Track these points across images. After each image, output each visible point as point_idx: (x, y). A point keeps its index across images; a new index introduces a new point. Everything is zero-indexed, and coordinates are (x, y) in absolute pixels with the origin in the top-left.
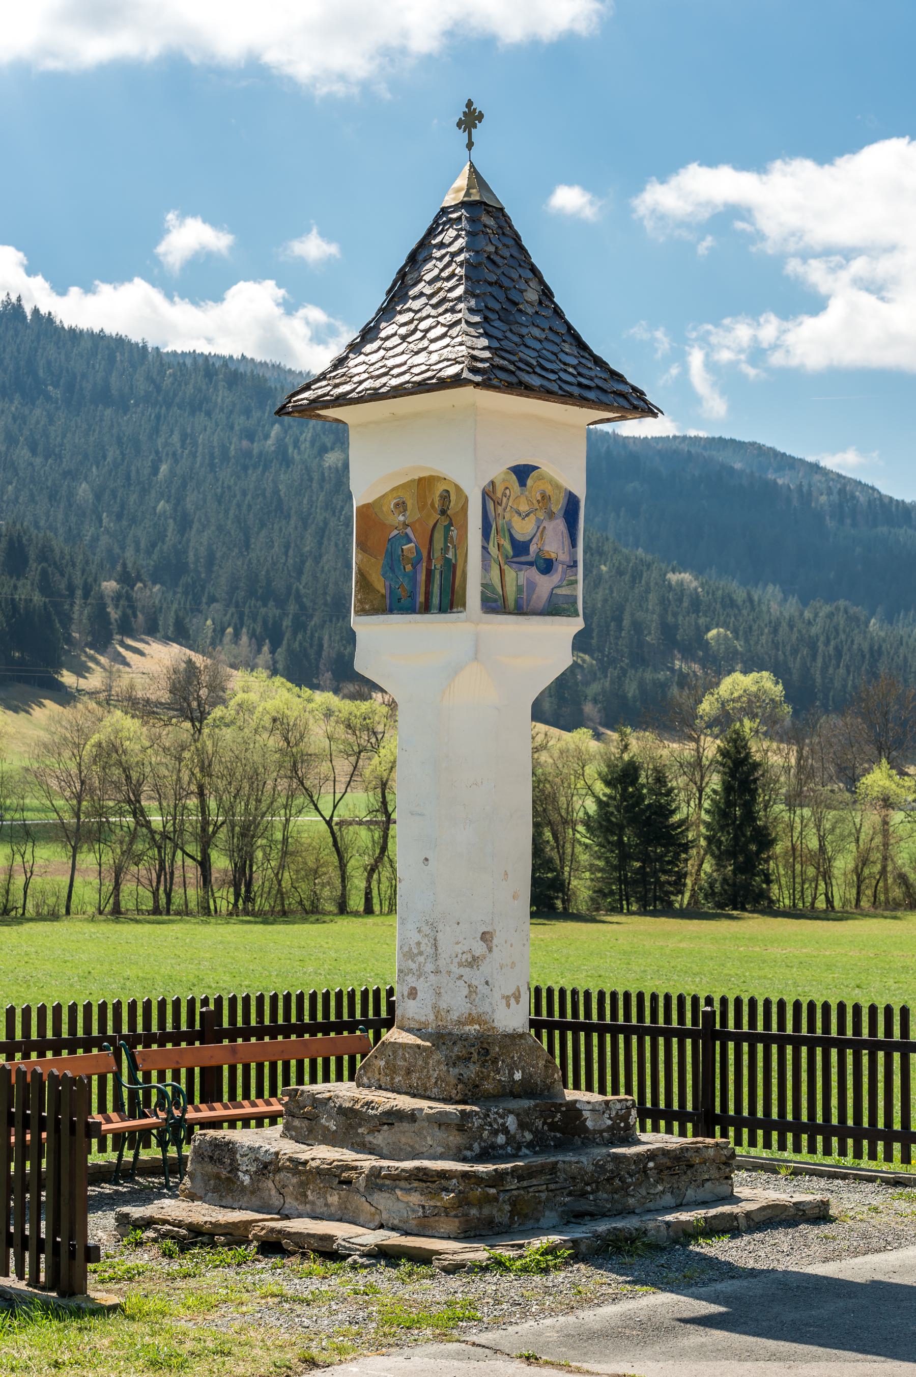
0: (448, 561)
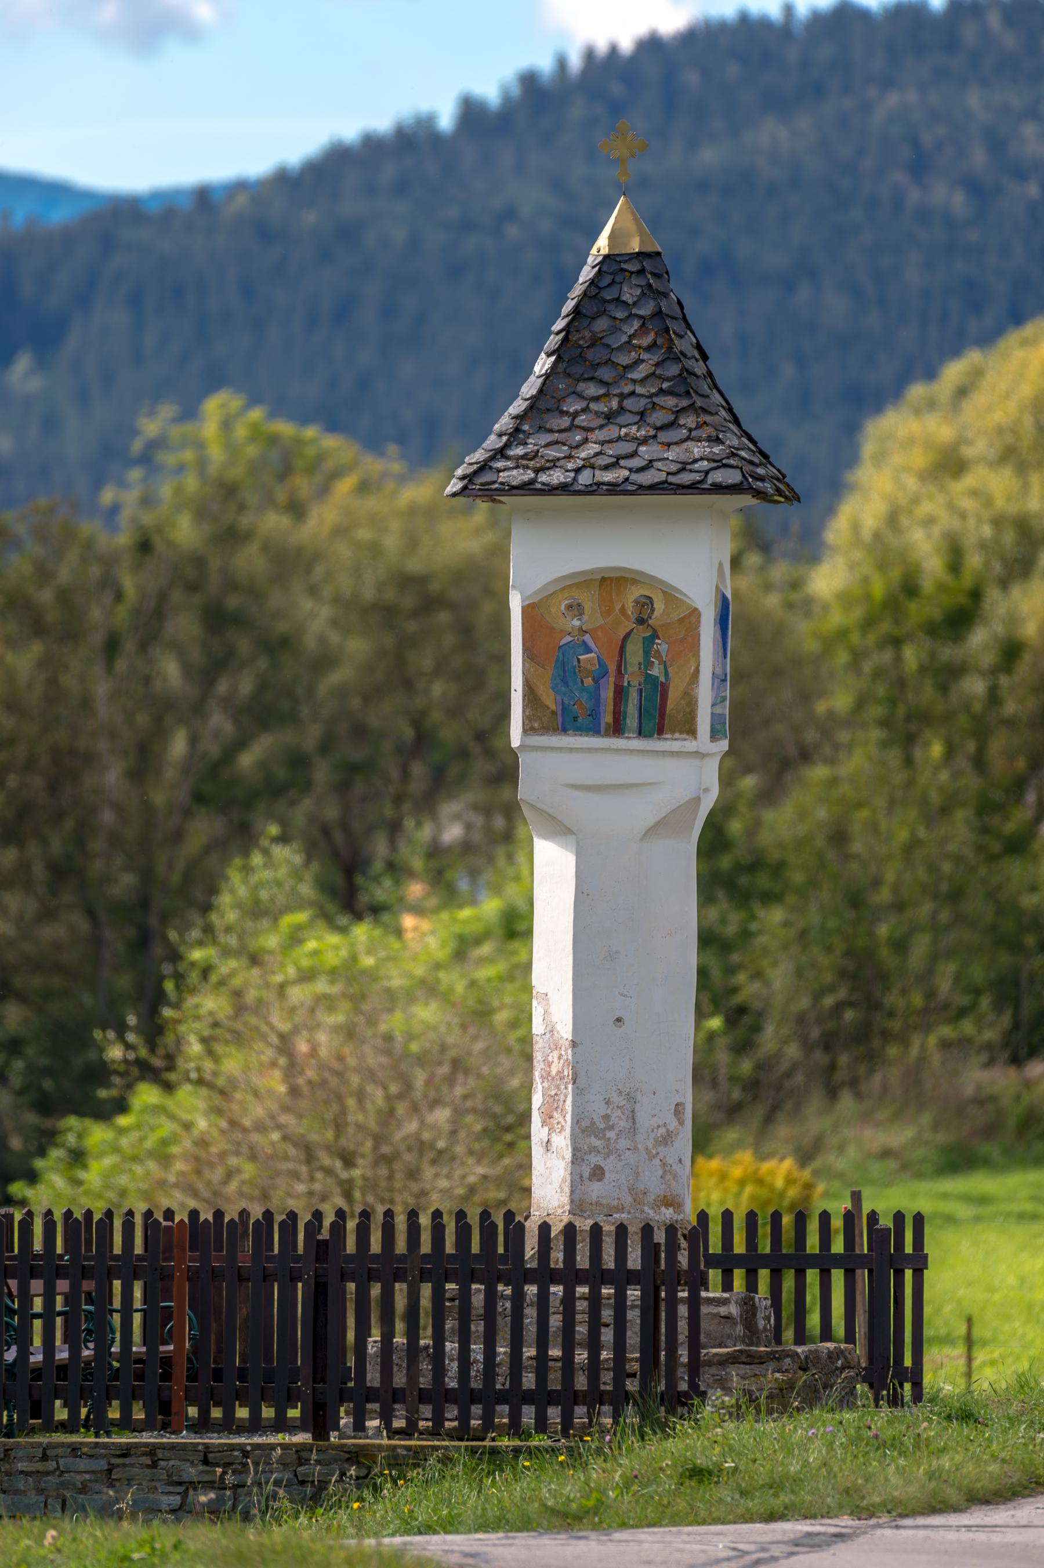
0: (651, 680)
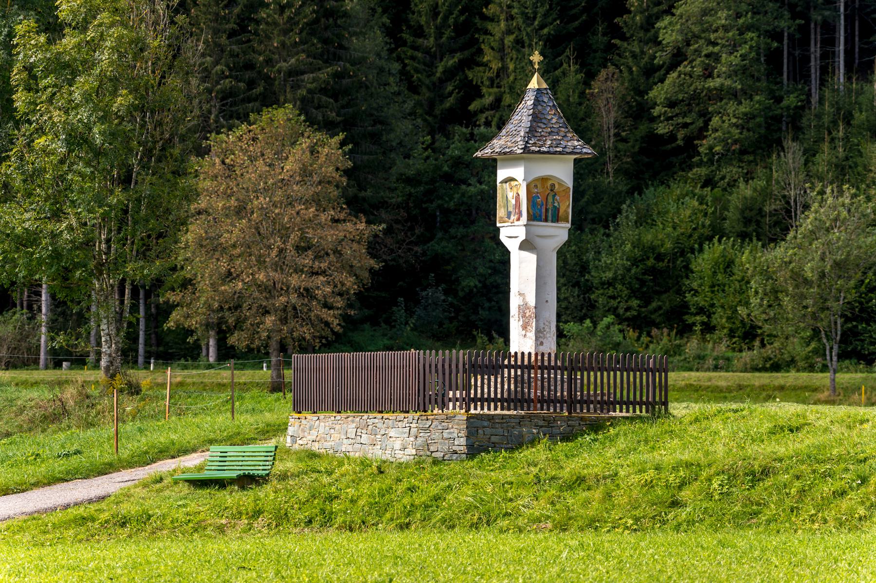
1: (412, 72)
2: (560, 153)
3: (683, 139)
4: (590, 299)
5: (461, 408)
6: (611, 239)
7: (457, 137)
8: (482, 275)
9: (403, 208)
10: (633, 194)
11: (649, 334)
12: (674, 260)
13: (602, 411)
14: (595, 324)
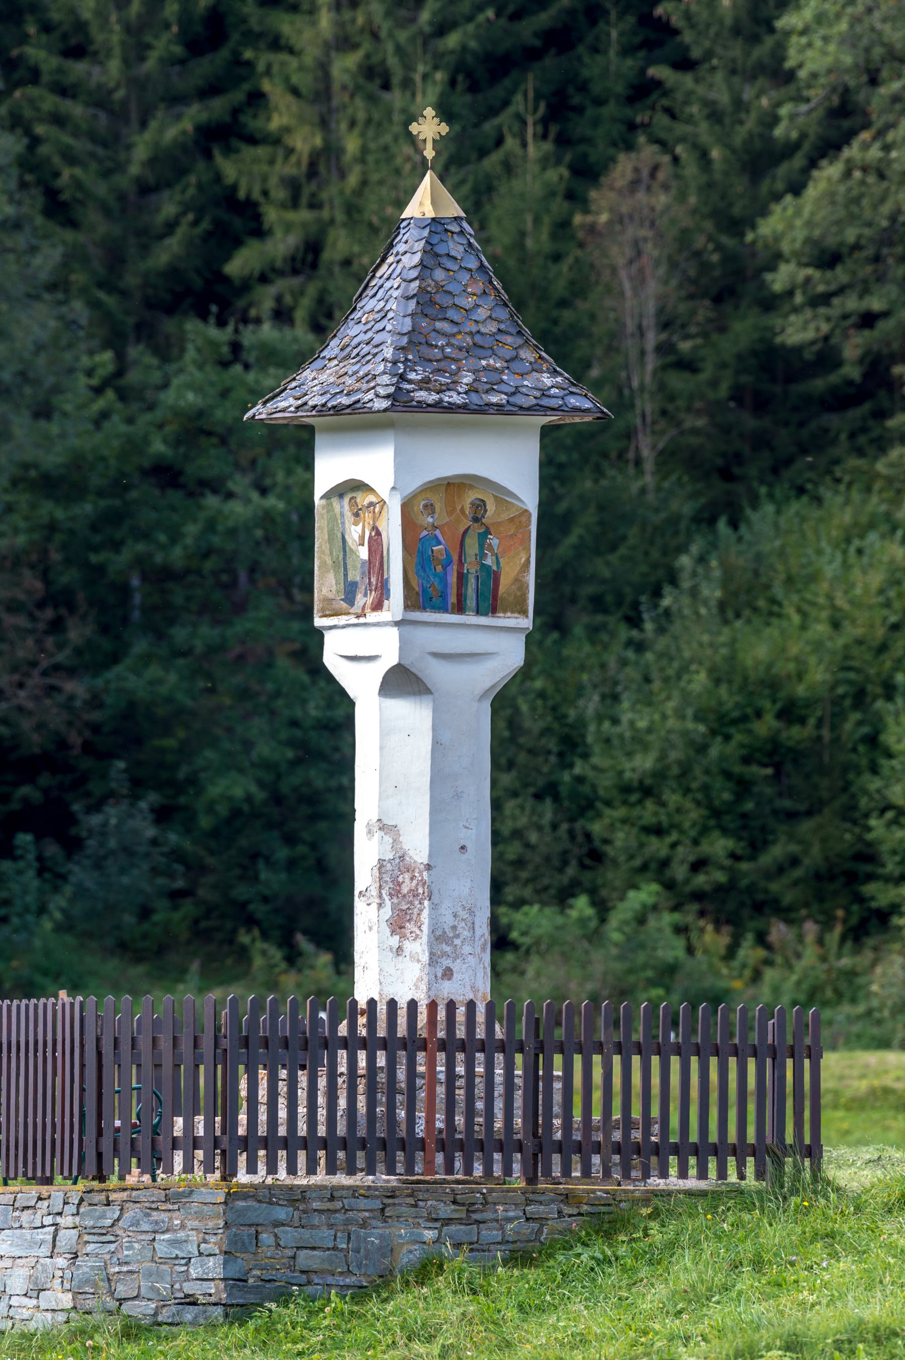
0: (485, 568)
1: (57, 160)
2: (499, 409)
3: (861, 361)
4: (588, 836)
5: (209, 1168)
6: (649, 656)
7: (191, 353)
8: (267, 765)
9: (32, 567)
10: (712, 521)
11: (761, 939)
12: (838, 717)
13: (626, 1175)
14: (603, 908)
